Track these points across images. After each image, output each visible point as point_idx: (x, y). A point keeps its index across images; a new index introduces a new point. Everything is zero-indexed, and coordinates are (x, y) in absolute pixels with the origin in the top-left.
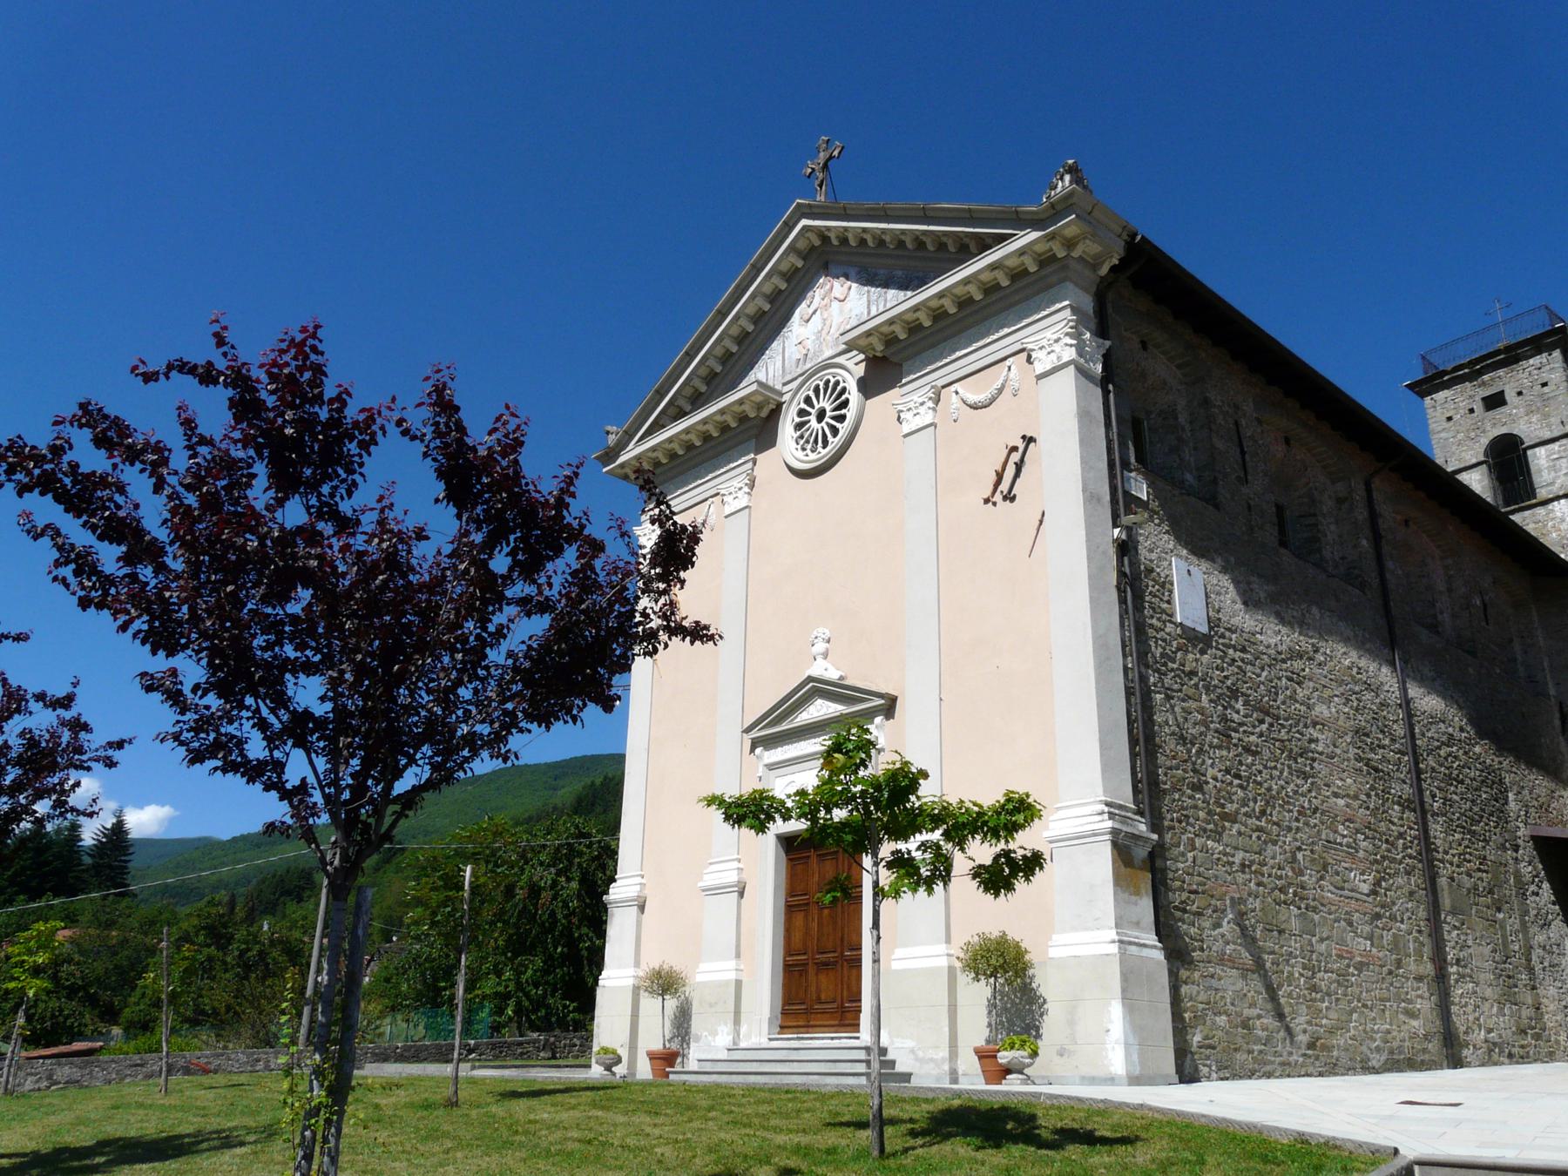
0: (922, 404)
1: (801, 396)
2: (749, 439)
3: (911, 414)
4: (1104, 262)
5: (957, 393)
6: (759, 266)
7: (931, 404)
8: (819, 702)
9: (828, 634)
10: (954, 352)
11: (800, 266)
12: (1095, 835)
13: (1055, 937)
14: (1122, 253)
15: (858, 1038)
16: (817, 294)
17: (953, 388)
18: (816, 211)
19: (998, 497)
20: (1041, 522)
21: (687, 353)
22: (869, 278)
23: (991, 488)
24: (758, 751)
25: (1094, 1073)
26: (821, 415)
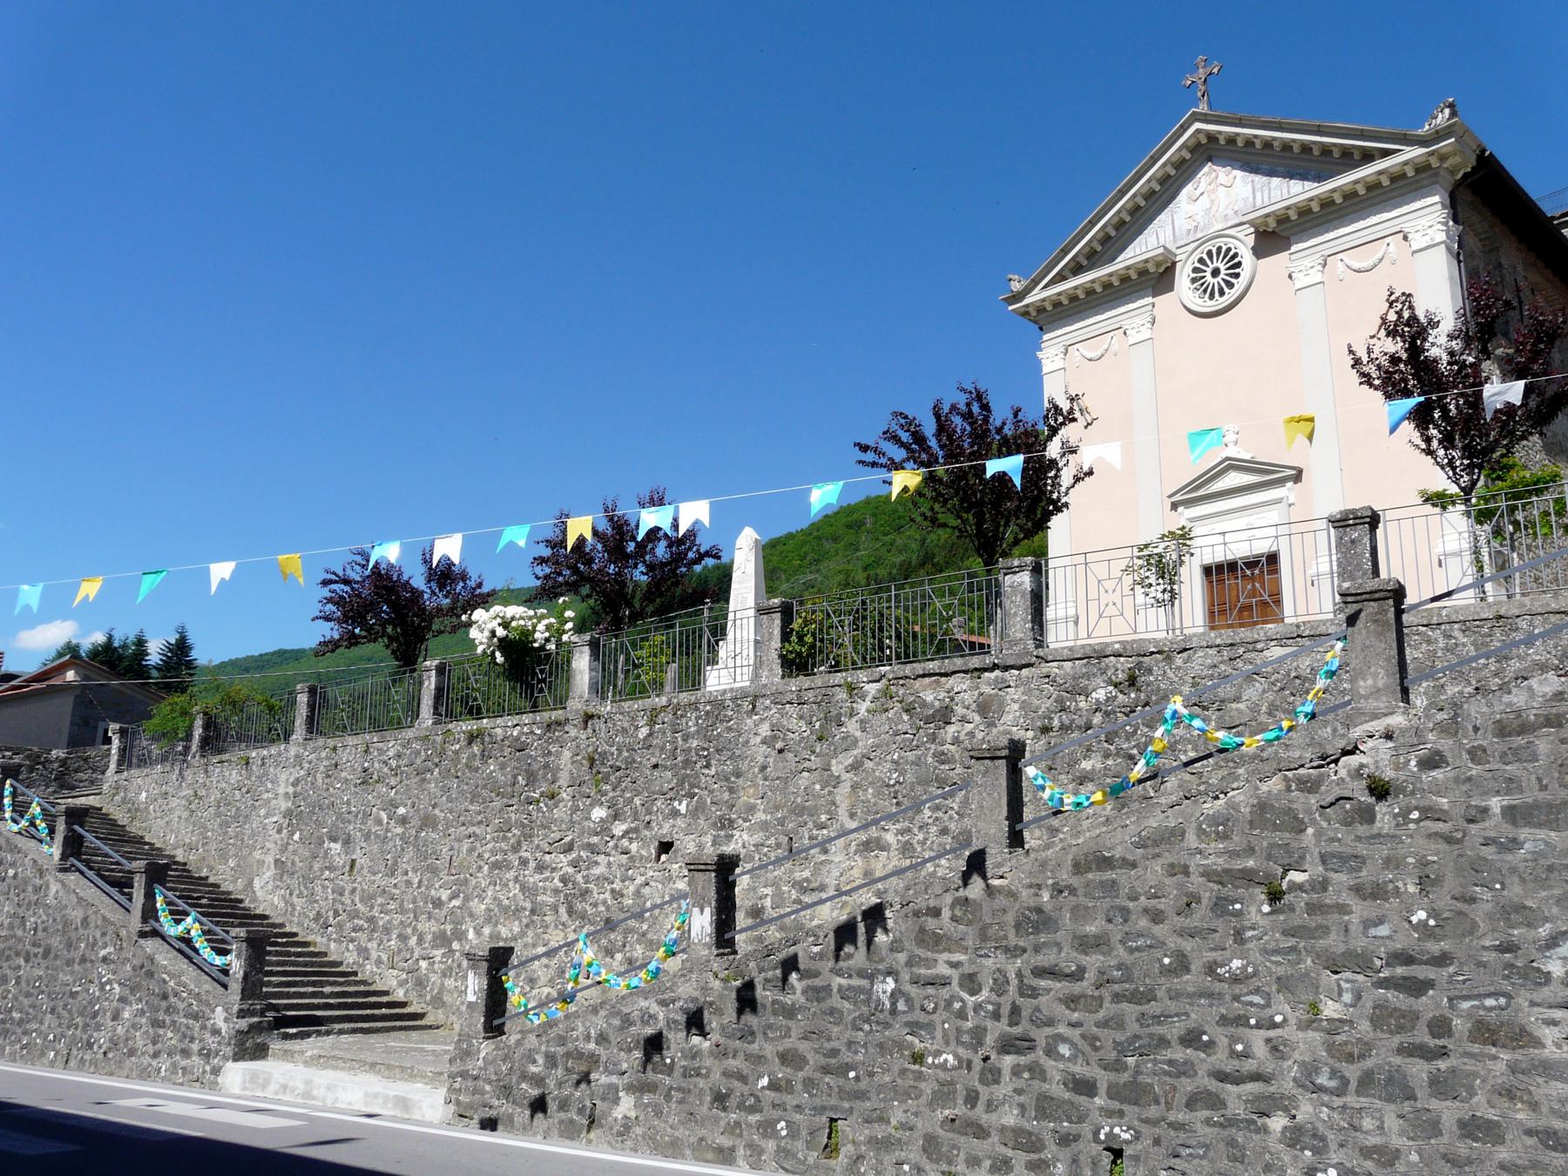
1: (1196, 256)
2: (1147, 288)
14: (1475, 163)
22: (1252, 167)
24: (1180, 509)
26: (1216, 273)
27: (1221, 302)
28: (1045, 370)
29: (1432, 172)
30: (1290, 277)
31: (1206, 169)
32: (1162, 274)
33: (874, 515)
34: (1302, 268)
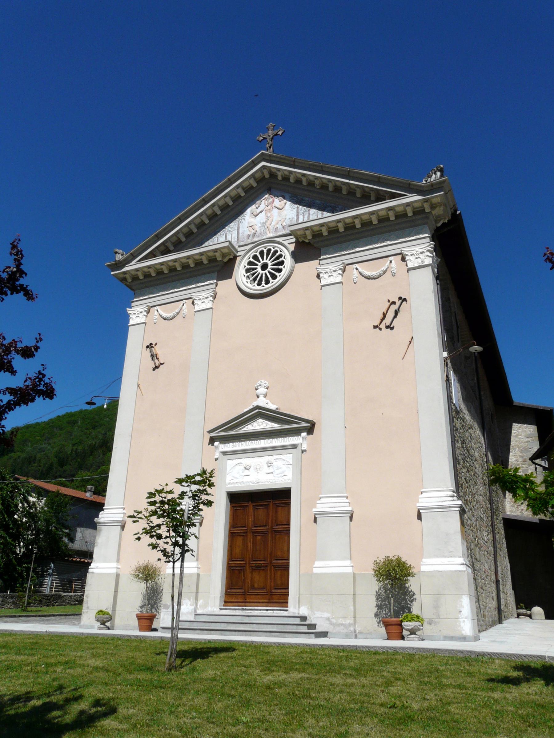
0: (141, 312)
1: (252, 254)
2: (214, 272)
3: (135, 316)
5: (157, 311)
7: (145, 313)
8: (260, 420)
9: (267, 384)
11: (254, 186)
12: (450, 507)
13: (424, 560)
15: (287, 610)
16: (263, 202)
18: (274, 159)
19: (383, 326)
20: (410, 342)
21: (179, 218)
22: (297, 200)
23: (379, 321)
24: (216, 443)
25: (451, 634)
26: (265, 267)
27: (265, 288)
28: (131, 322)
29: (424, 216)
30: (318, 276)
31: (266, 196)
33: (83, 419)
34: (328, 270)
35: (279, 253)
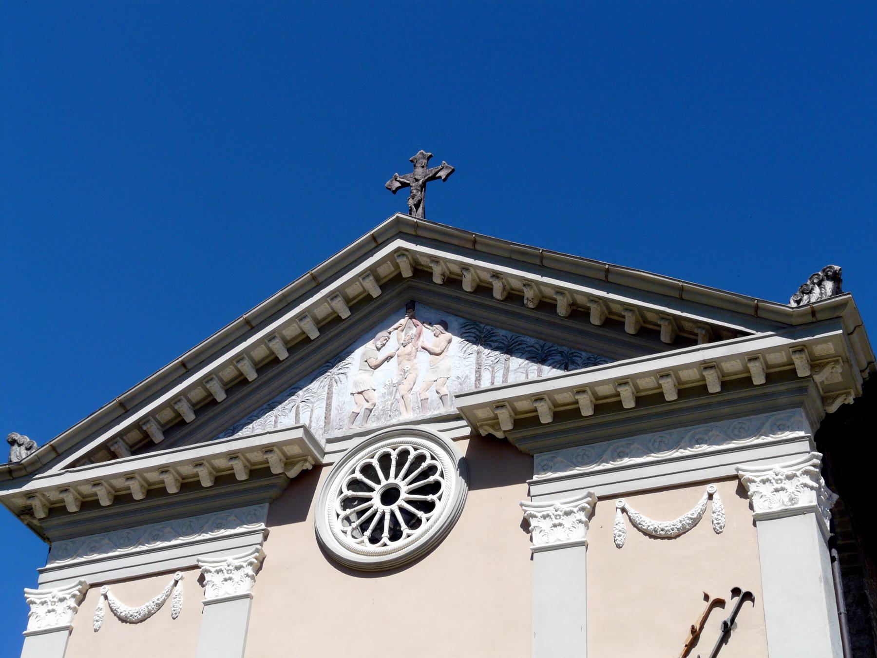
0: (62, 600)
1: (360, 460)
2: (259, 502)
4: (838, 396)
5: (106, 597)
6: (321, 279)
10: (621, 456)
16: (394, 334)
17: (102, 590)
21: (183, 364)
26: (390, 496)
29: (793, 385)
31: (402, 321)
32: (294, 481)
34: (551, 511)
35: (428, 462)
